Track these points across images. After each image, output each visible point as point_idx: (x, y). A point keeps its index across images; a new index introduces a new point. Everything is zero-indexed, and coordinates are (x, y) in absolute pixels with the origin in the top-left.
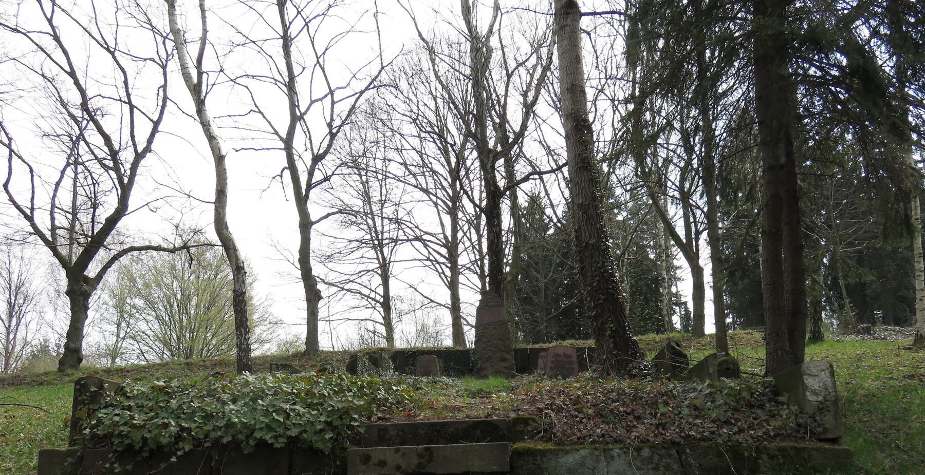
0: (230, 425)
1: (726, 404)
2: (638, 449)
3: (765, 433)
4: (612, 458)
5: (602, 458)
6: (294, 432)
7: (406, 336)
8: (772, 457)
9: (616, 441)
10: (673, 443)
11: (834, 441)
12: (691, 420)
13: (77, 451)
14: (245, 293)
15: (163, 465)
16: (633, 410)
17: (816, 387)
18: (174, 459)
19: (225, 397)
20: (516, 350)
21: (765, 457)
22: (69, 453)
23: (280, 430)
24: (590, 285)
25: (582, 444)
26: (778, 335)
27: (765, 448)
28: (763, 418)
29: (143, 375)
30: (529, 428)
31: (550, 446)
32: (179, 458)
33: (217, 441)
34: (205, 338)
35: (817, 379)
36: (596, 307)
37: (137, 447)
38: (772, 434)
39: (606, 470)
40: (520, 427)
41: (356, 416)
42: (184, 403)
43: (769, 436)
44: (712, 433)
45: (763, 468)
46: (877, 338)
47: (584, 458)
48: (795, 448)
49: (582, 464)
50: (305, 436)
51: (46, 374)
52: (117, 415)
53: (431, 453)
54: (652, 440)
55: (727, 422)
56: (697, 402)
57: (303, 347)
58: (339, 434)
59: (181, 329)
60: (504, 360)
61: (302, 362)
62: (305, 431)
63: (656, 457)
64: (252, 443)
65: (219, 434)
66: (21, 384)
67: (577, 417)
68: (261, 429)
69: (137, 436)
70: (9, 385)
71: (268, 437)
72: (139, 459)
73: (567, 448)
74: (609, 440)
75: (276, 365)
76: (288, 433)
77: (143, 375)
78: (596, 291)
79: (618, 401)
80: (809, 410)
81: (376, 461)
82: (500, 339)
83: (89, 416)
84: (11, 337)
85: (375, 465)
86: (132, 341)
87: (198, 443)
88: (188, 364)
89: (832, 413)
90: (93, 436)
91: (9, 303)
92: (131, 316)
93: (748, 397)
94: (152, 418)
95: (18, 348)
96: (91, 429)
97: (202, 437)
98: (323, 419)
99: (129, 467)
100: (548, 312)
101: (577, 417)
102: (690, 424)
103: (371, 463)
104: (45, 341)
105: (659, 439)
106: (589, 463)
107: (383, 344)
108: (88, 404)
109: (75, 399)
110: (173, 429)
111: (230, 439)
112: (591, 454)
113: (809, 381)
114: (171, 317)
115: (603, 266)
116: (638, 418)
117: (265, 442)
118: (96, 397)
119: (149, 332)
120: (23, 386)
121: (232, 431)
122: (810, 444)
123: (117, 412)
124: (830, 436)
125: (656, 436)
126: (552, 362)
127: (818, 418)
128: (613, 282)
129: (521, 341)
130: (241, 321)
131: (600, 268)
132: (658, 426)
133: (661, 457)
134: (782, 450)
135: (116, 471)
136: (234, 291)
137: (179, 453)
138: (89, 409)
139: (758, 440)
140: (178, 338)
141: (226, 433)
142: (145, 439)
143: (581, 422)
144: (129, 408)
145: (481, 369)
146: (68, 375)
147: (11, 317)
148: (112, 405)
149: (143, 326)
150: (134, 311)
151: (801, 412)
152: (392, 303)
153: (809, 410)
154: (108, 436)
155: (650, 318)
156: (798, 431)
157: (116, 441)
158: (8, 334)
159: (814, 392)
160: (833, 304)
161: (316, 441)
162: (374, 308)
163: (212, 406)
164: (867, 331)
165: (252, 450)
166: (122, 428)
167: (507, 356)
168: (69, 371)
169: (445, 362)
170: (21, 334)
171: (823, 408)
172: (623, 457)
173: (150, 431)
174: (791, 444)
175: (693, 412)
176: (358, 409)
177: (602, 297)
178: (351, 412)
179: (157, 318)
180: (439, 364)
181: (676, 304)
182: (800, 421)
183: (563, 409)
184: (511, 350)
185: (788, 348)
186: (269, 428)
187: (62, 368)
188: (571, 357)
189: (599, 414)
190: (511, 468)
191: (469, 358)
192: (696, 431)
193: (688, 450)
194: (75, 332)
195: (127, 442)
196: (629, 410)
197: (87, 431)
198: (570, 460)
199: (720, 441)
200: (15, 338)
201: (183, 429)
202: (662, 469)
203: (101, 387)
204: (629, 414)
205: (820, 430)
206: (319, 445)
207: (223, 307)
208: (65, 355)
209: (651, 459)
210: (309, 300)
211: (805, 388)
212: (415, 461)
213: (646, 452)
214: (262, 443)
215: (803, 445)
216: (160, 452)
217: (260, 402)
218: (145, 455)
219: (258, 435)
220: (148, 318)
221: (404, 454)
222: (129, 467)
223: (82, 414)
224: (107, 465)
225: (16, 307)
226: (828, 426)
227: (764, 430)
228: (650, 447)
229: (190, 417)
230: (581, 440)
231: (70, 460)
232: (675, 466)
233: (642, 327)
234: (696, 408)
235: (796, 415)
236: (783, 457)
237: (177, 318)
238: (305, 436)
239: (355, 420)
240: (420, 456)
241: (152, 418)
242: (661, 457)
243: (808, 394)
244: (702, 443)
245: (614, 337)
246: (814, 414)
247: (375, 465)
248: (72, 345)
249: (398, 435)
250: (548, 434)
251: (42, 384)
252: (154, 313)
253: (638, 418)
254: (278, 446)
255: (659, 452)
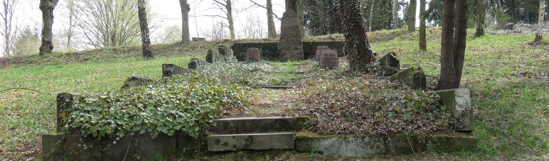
0: (143, 124)
1: (412, 110)
2: (363, 138)
3: (431, 129)
4: (349, 142)
5: (344, 142)
6: (178, 128)
7: (242, 34)
8: (434, 143)
9: (352, 133)
10: (382, 134)
11: (469, 132)
12: (392, 120)
13: (61, 136)
14: (145, 8)
15: (109, 146)
16: (362, 113)
17: (461, 103)
18: (115, 142)
19: (140, 105)
20: (304, 43)
21: (430, 142)
22: (59, 137)
23: (171, 127)
24: (346, 17)
25: (333, 134)
26: (448, 59)
27: (431, 137)
28: (432, 119)
29: (89, 57)
30: (305, 123)
31: (316, 135)
32: (117, 141)
33: (137, 132)
34: (122, 25)
35: (463, 98)
36: (348, 30)
37: (95, 136)
38: (435, 130)
39: (345, 148)
40: (300, 123)
41: (211, 117)
42: (118, 110)
43: (433, 131)
44: (403, 129)
45: (429, 148)
46: (516, 32)
47: (334, 142)
48: (447, 138)
49: (333, 145)
50: (184, 129)
51: (33, 56)
52: (82, 116)
53: (252, 138)
54: (370, 132)
55: (412, 122)
56: (397, 109)
57: (181, 39)
58: (202, 128)
59: (108, 20)
60: (297, 49)
61: (180, 48)
62: (184, 127)
63: (372, 142)
64: (156, 134)
65: (138, 129)
66: (19, 63)
67: (331, 116)
68: (161, 126)
69: (94, 130)
70: (12, 63)
71: (165, 131)
72: (96, 141)
73: (326, 137)
74: (347, 132)
75: (166, 65)
76: (175, 128)
77: (89, 57)
78: (349, 21)
79: (354, 106)
80: (457, 115)
81: (223, 143)
82: (295, 37)
83: (66, 115)
84: (8, 24)
85: (222, 145)
86: (79, 27)
87: (126, 132)
88: (114, 50)
89: (469, 117)
90: (70, 128)
91: (5, 4)
92: (77, 11)
93: (425, 106)
94: (101, 119)
95: (13, 31)
96: (69, 124)
97: (129, 129)
98: (193, 119)
99: (91, 146)
100: (325, 10)
101: (331, 116)
102: (392, 123)
103: (221, 143)
104: (28, 26)
105: (375, 132)
106: (337, 144)
107: (226, 34)
108: (65, 108)
109: (58, 106)
110: (113, 126)
111: (144, 131)
112: (338, 140)
113: (458, 100)
114: (101, 12)
115: (354, 6)
116: (364, 118)
117: (163, 133)
118: (69, 105)
119: (89, 22)
120: (21, 64)
121: (145, 127)
122: (454, 135)
123: (82, 114)
124: (467, 130)
125: (373, 130)
126: (323, 59)
127: (461, 120)
128: (359, 15)
129: (308, 36)
130: (144, 25)
131: (352, 7)
132: (374, 124)
133: (375, 141)
134: (439, 139)
135: (85, 148)
136: (139, 8)
137: (117, 139)
138: (66, 112)
139: (428, 133)
140: (107, 26)
141: (142, 128)
142: (98, 131)
143: (333, 120)
144: (88, 112)
145: (284, 54)
146: (45, 57)
147: (6, 12)
148: (78, 109)
149: (84, 18)
150: (79, 9)
151: (452, 117)
152: (232, 6)
153: (457, 115)
154: (79, 128)
155: (385, 13)
156: (450, 128)
157: (83, 132)
158: (6, 23)
159: (460, 106)
160: (495, 5)
161: (191, 133)
162: (221, 9)
163: (133, 111)
164: (511, 27)
165: (156, 137)
166: (85, 125)
167: (299, 47)
168: (46, 55)
169: (263, 50)
170: (13, 23)
171: (464, 115)
172: (354, 142)
173: (101, 127)
174: (445, 135)
175: (394, 115)
176: (213, 112)
177: (353, 25)
178: (209, 115)
179: (93, 13)
180: (259, 51)
181: (402, 4)
182: (451, 122)
183: (324, 111)
184: (301, 43)
185: (453, 67)
186: (165, 125)
187: (42, 53)
188: (334, 55)
189: (344, 115)
190: (295, 147)
191: (277, 48)
192: (395, 128)
193: (389, 139)
194: (47, 30)
195: (89, 133)
196: (359, 113)
197: (67, 126)
198: (326, 143)
199: (407, 134)
200: (10, 25)
201: (118, 125)
202: (375, 148)
203: (71, 99)
204: (359, 115)
205: (461, 126)
206: (192, 135)
207: (132, 7)
208: (43, 45)
209: (369, 142)
210: (183, 11)
211: (456, 103)
212: (244, 143)
213: (367, 139)
214: (161, 134)
215: (451, 136)
216: (107, 139)
217: (159, 109)
218: (99, 139)
219: (159, 129)
220: (88, 13)
221: (237, 139)
222: (91, 146)
223: (63, 115)
224: (80, 145)
225: (9, 6)
226: (466, 124)
227: (431, 127)
228: (369, 137)
229: (122, 118)
230: (332, 132)
231: (59, 141)
232: (382, 147)
233: (381, 18)
234: (396, 112)
235: (450, 118)
236: (440, 142)
237: (104, 12)
238: (184, 129)
239: (211, 119)
240: (246, 140)
241: (101, 119)
242: (375, 141)
243: (457, 107)
244: (398, 134)
245: (358, 48)
246: (459, 118)
247: (222, 145)
248: (46, 39)
249: (234, 126)
250: (314, 127)
251: (31, 63)
252: (91, 11)
253: (364, 118)
254: (170, 135)
255: (374, 139)
